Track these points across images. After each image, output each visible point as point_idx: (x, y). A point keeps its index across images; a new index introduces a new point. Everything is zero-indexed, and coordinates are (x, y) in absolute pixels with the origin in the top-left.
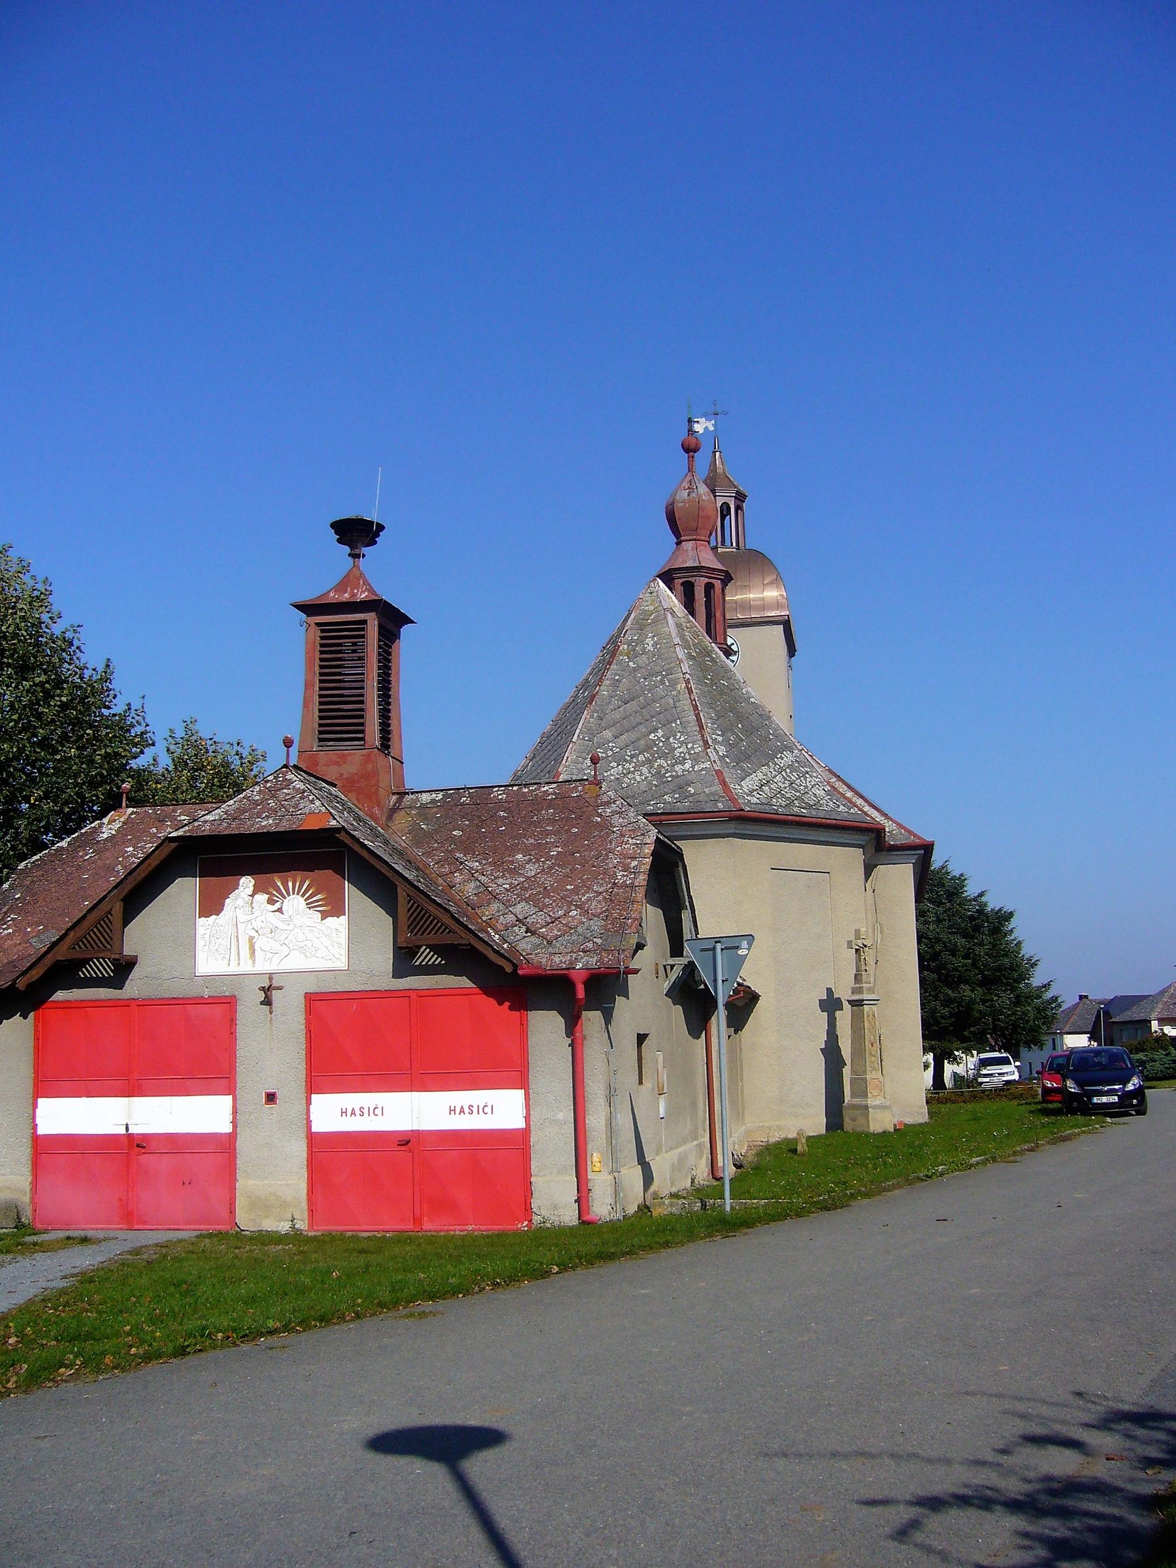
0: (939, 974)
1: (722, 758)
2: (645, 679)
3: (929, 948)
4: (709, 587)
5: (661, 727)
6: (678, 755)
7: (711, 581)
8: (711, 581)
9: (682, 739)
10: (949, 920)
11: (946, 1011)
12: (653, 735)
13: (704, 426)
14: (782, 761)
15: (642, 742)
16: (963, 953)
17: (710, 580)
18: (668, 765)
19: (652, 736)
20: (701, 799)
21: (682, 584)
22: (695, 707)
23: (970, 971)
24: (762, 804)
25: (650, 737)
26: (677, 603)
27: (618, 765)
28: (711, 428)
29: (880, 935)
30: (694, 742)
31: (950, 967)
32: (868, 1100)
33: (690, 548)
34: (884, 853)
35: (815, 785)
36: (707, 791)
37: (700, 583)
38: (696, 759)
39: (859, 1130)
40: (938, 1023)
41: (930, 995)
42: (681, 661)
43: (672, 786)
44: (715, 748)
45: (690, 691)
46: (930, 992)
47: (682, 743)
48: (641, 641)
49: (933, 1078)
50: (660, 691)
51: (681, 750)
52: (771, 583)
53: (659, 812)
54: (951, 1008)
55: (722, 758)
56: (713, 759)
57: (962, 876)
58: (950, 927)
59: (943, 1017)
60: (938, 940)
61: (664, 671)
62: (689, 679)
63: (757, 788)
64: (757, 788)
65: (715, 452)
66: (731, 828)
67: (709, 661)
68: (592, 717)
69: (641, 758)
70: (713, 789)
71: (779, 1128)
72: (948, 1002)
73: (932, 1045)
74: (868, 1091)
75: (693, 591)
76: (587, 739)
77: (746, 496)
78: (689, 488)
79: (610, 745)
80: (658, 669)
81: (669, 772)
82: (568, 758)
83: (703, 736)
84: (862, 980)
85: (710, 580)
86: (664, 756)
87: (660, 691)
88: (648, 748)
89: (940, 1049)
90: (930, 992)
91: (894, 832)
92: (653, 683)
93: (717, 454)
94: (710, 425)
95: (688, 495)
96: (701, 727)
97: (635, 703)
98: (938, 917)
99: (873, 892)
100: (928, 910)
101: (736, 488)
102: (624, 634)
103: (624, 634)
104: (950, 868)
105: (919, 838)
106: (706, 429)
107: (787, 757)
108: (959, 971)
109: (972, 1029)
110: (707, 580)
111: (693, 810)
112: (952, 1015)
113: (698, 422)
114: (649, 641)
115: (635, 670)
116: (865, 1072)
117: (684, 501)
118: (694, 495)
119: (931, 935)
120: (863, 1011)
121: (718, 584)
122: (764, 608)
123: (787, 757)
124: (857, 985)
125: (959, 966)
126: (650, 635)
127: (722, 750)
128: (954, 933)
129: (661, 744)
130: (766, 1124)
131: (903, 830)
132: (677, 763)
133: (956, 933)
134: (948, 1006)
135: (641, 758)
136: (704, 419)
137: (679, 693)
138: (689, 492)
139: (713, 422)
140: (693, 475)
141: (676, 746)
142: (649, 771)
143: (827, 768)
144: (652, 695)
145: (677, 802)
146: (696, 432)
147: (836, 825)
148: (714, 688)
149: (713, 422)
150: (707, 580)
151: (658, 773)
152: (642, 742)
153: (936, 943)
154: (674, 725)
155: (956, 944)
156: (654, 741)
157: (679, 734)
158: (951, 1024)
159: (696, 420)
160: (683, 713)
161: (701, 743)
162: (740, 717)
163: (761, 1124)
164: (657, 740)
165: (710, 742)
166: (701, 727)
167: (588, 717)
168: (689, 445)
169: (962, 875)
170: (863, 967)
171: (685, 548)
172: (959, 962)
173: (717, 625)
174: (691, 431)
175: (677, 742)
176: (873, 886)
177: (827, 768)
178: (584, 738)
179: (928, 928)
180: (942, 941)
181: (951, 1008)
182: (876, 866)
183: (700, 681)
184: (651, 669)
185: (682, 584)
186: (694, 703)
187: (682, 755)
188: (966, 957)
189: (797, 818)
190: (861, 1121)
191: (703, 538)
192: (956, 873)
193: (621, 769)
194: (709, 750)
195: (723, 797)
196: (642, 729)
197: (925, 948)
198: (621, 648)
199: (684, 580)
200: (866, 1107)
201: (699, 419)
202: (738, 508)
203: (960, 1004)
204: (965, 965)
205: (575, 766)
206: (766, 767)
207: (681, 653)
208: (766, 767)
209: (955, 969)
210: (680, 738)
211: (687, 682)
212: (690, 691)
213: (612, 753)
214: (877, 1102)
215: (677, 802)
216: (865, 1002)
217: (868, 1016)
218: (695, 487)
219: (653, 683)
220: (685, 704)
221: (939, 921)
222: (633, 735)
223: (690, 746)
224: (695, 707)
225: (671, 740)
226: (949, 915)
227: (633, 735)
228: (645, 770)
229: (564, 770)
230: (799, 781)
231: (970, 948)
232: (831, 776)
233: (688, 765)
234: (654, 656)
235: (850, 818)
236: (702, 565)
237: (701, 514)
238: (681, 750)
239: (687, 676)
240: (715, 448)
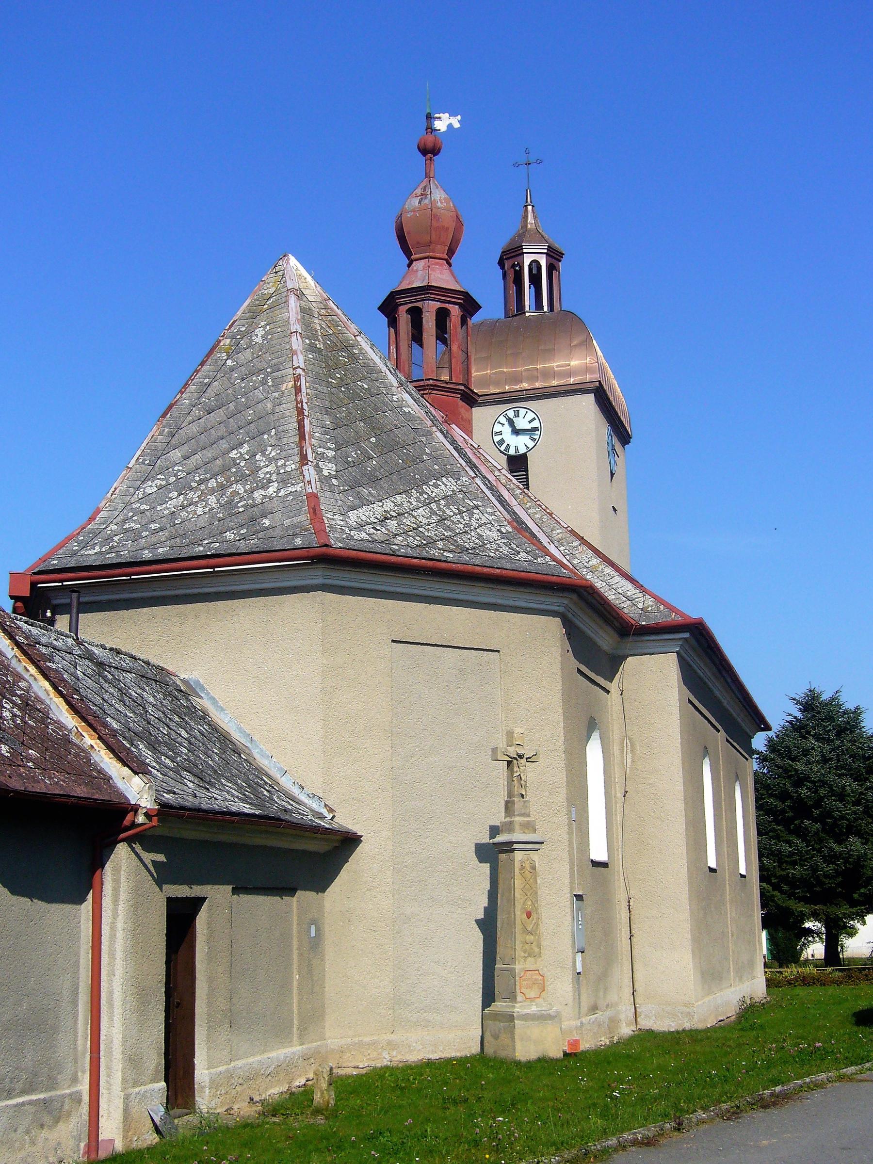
0: (824, 824)
1: (325, 480)
2: (243, 379)
3: (813, 793)
4: (442, 316)
5: (248, 441)
6: (262, 476)
7: (447, 306)
8: (447, 306)
9: (273, 454)
10: (838, 761)
11: (830, 869)
12: (235, 452)
13: (448, 123)
14: (436, 490)
15: (219, 462)
16: (853, 799)
17: (444, 305)
18: (246, 491)
19: (233, 454)
20: (275, 534)
21: (409, 311)
22: (300, 411)
23: (862, 819)
24: (374, 541)
25: (230, 455)
26: (313, 285)
27: (179, 495)
28: (457, 125)
29: (630, 755)
30: (287, 458)
31: (836, 814)
32: (517, 1005)
33: (421, 268)
34: (631, 638)
35: (485, 524)
36: (287, 522)
37: (430, 309)
38: (284, 481)
39: (503, 1054)
40: (820, 883)
41: (813, 849)
42: (294, 353)
43: (241, 519)
44: (317, 466)
45: (298, 390)
46: (813, 846)
47: (271, 460)
48: (249, 333)
49: (165, 1029)
50: (259, 394)
51: (268, 470)
52: (580, 345)
53: (208, 553)
54: (837, 865)
55: (325, 480)
56: (307, 478)
57: (858, 709)
58: (837, 768)
59: (826, 876)
60: (823, 783)
61: (269, 367)
62: (300, 375)
63: (376, 520)
64: (376, 520)
65: (526, 206)
66: (317, 575)
67: (344, 357)
68: (161, 434)
69: (212, 483)
70: (296, 520)
71: (391, 1045)
72: (831, 858)
73: (815, 910)
74: (518, 991)
75: (421, 319)
76: (147, 462)
77: (564, 254)
78: (422, 195)
79: (176, 468)
80: (264, 365)
81: (245, 500)
82: (116, 489)
83: (301, 448)
84: (514, 811)
85: (444, 305)
86: (242, 479)
87: (259, 394)
88: (225, 469)
89: (825, 914)
90: (813, 846)
91: (650, 609)
92: (251, 384)
93: (530, 208)
94: (456, 122)
95: (420, 202)
96: (302, 437)
97: (222, 412)
98: (823, 756)
99: (621, 694)
100: (813, 748)
101: (547, 243)
102: (230, 327)
103: (230, 327)
104: (842, 700)
105: (682, 614)
106: (450, 126)
107: (446, 486)
108: (848, 820)
109: (862, 891)
110: (438, 305)
111: (258, 549)
112: (838, 873)
113: (440, 118)
114: (260, 332)
115: (232, 369)
116: (513, 960)
117: (413, 211)
118: (427, 201)
119: (813, 777)
120: (513, 861)
121: (455, 311)
122: (569, 374)
123: (446, 486)
124: (508, 819)
125: (848, 814)
126: (262, 324)
127: (328, 469)
128: (843, 775)
129: (242, 464)
130: (367, 1039)
131: (662, 607)
132: (258, 488)
133: (846, 775)
134: (833, 863)
135: (212, 483)
136: (447, 115)
137: (283, 393)
138: (422, 199)
139: (459, 117)
140: (430, 181)
141: (262, 464)
142: (218, 500)
143: (569, 529)
144: (247, 399)
145: (239, 540)
146: (437, 130)
147: (502, 576)
148: (343, 389)
149: (459, 117)
150: (438, 305)
151: (230, 502)
152: (219, 462)
153: (820, 787)
154: (266, 437)
155: (844, 787)
156: (234, 459)
157: (270, 449)
158: (838, 885)
159: (437, 115)
160: (282, 421)
161: (297, 458)
162: (376, 429)
163: (356, 1040)
164: (238, 458)
165: (310, 457)
166: (302, 437)
167: (157, 434)
168: (425, 144)
169: (857, 708)
170: (517, 790)
171: (415, 268)
172: (849, 810)
173: (453, 361)
174: (431, 129)
175: (264, 459)
176: (620, 685)
177: (569, 529)
178: (144, 460)
179: (811, 769)
180: (827, 784)
181: (837, 865)
182: (625, 658)
183: (317, 379)
184: (253, 366)
185: (409, 311)
186: (299, 405)
187: (268, 476)
188: (857, 803)
189: (429, 563)
190: (504, 1038)
191: (438, 255)
192: (850, 706)
193: (182, 500)
194: (306, 467)
195: (306, 530)
196: (224, 445)
197: (807, 792)
198: (221, 344)
199: (410, 305)
200: (511, 1018)
201: (441, 115)
202: (551, 268)
203: (846, 861)
204: (855, 813)
205: (120, 499)
206: (404, 496)
207: (296, 343)
208: (404, 496)
209: (842, 817)
210: (270, 453)
211: (297, 378)
212: (298, 390)
213: (175, 479)
214: (533, 1009)
215: (239, 540)
216: (516, 846)
217: (522, 868)
218: (429, 193)
219: (251, 384)
220: (288, 408)
221: (825, 760)
222: (209, 454)
223: (280, 463)
224: (300, 411)
225: (258, 457)
226: (838, 755)
227: (209, 454)
228: (212, 500)
229: (107, 505)
230: (458, 516)
231: (862, 793)
232: (572, 538)
233: (271, 490)
234: (260, 350)
235: (532, 569)
236: (433, 284)
237: (435, 224)
238: (268, 470)
239: (299, 371)
240: (527, 202)
